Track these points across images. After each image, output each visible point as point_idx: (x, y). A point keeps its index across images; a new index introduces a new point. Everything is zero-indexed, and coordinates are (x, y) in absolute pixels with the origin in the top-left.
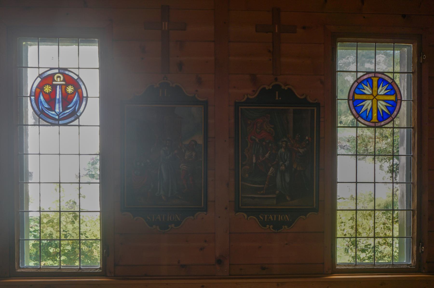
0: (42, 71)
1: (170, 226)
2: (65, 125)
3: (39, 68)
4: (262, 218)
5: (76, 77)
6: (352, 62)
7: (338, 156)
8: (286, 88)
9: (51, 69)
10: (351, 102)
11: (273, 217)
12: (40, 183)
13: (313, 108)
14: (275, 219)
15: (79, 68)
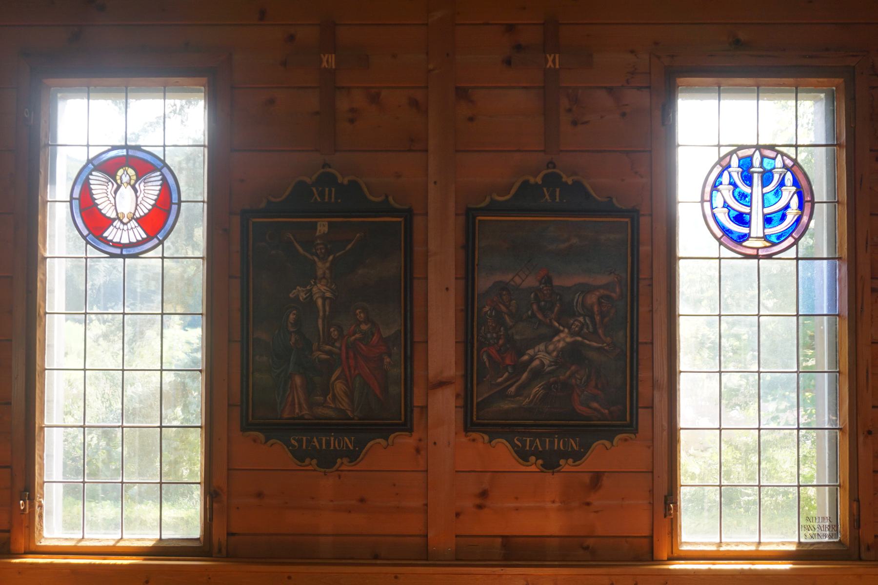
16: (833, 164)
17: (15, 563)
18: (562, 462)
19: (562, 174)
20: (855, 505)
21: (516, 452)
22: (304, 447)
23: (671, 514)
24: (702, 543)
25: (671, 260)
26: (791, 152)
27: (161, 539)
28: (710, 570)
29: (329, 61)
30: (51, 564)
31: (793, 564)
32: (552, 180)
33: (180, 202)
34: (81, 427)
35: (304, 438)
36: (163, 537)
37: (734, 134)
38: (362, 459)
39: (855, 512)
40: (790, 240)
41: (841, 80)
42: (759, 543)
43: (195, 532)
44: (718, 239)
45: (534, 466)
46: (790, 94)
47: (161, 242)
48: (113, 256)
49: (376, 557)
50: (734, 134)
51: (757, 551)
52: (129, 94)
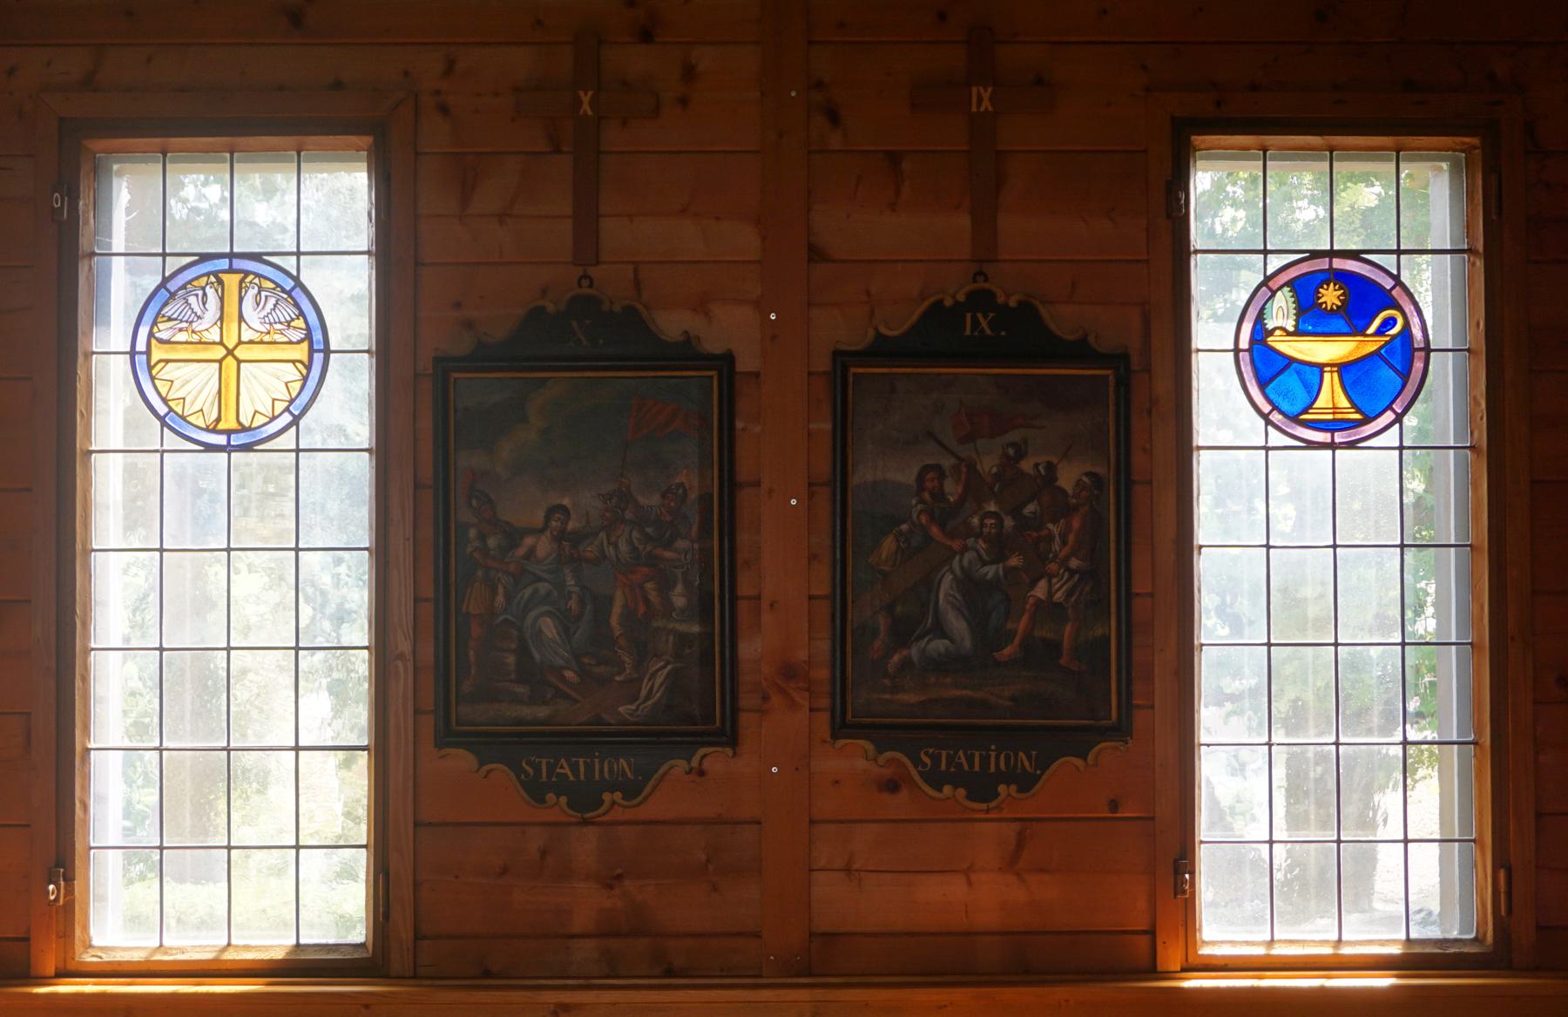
1: (607, 797)
2: (1351, 445)
3: (1265, 252)
4: (530, 770)
5: (1388, 283)
6: (1250, 215)
11: (970, 760)
13: (851, 380)
14: (977, 768)
17: (37, 995)
20: (1502, 874)
21: (522, 783)
22: (943, 767)
23: (1184, 892)
24: (1247, 943)
25: (384, 451)
26: (289, 263)
27: (298, 945)
28: (1322, 989)
29: (982, 98)
31: (1398, 977)
34: (223, 749)
35: (544, 761)
36: (302, 941)
38: (645, 799)
40: (1389, 417)
41: (1475, 141)
42: (1340, 940)
43: (358, 934)
47: (1399, 419)
49: (487, 974)
51: (1268, 956)
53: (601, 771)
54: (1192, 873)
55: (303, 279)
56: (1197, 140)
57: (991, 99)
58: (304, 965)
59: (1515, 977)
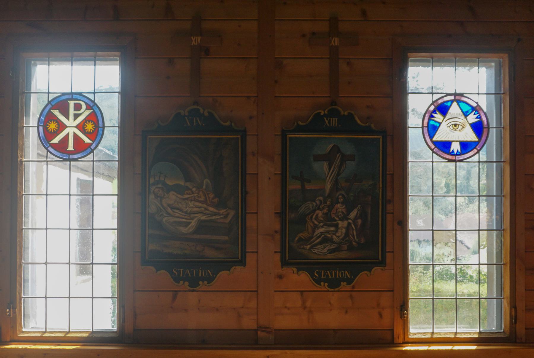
0: (436, 97)
6: (426, 81)
7: (117, 193)
8: (346, 113)
9: (448, 95)
10: (426, 129)
11: (192, 273)
12: (46, 229)
14: (333, 277)
15: (478, 94)
16: (499, 104)
18: (201, 283)
19: (339, 109)
22: (181, 275)
23: (404, 317)
26: (91, 96)
30: (26, 349)
32: (333, 113)
33: (104, 127)
37: (449, 89)
39: (513, 314)
44: (432, 150)
45: (324, 286)
46: (89, 62)
48: (450, 161)
50: (449, 89)
52: (73, 62)
53: (202, 273)
54: (407, 310)
55: (96, 102)
56: (409, 54)
57: (192, 41)
58: (96, 338)
59: (502, 346)
